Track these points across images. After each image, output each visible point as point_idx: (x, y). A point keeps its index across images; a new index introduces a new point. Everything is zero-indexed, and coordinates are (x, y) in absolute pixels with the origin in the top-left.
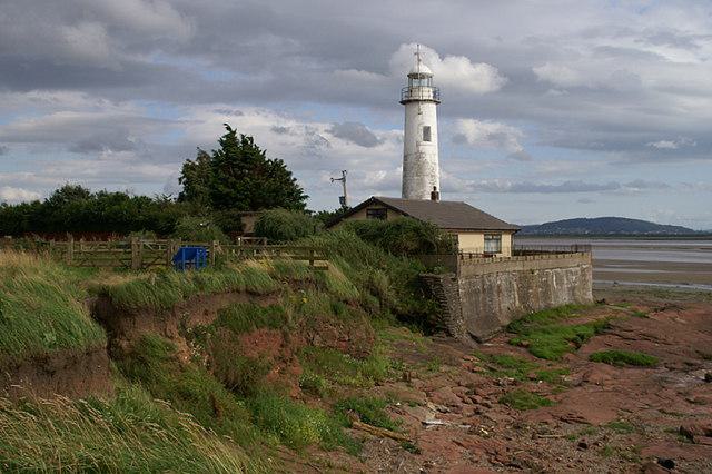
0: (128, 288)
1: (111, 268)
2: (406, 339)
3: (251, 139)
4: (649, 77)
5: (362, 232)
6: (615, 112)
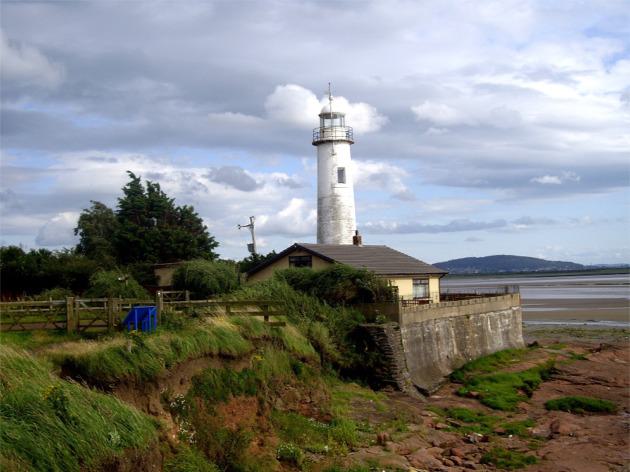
0: (101, 358)
2: (362, 396)
3: (157, 186)
4: (530, 112)
5: (295, 283)
6: (496, 148)
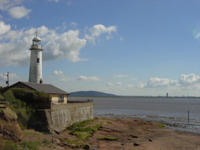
1: (18, 103)
